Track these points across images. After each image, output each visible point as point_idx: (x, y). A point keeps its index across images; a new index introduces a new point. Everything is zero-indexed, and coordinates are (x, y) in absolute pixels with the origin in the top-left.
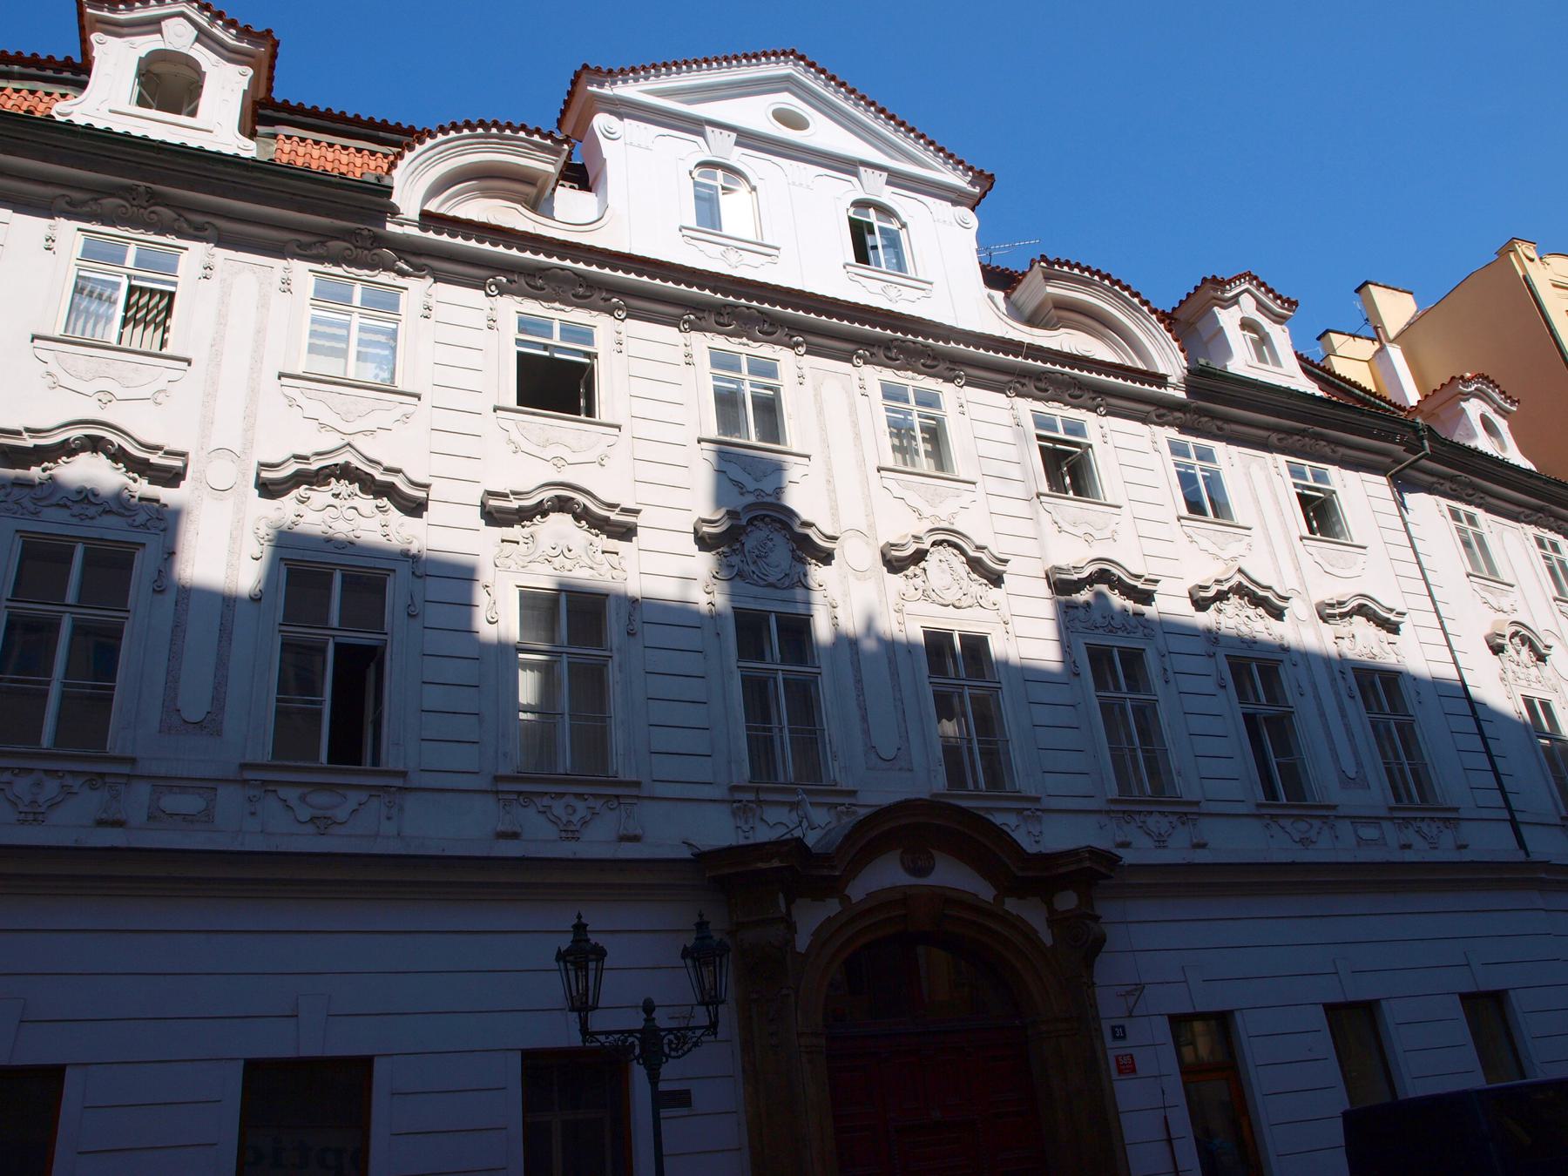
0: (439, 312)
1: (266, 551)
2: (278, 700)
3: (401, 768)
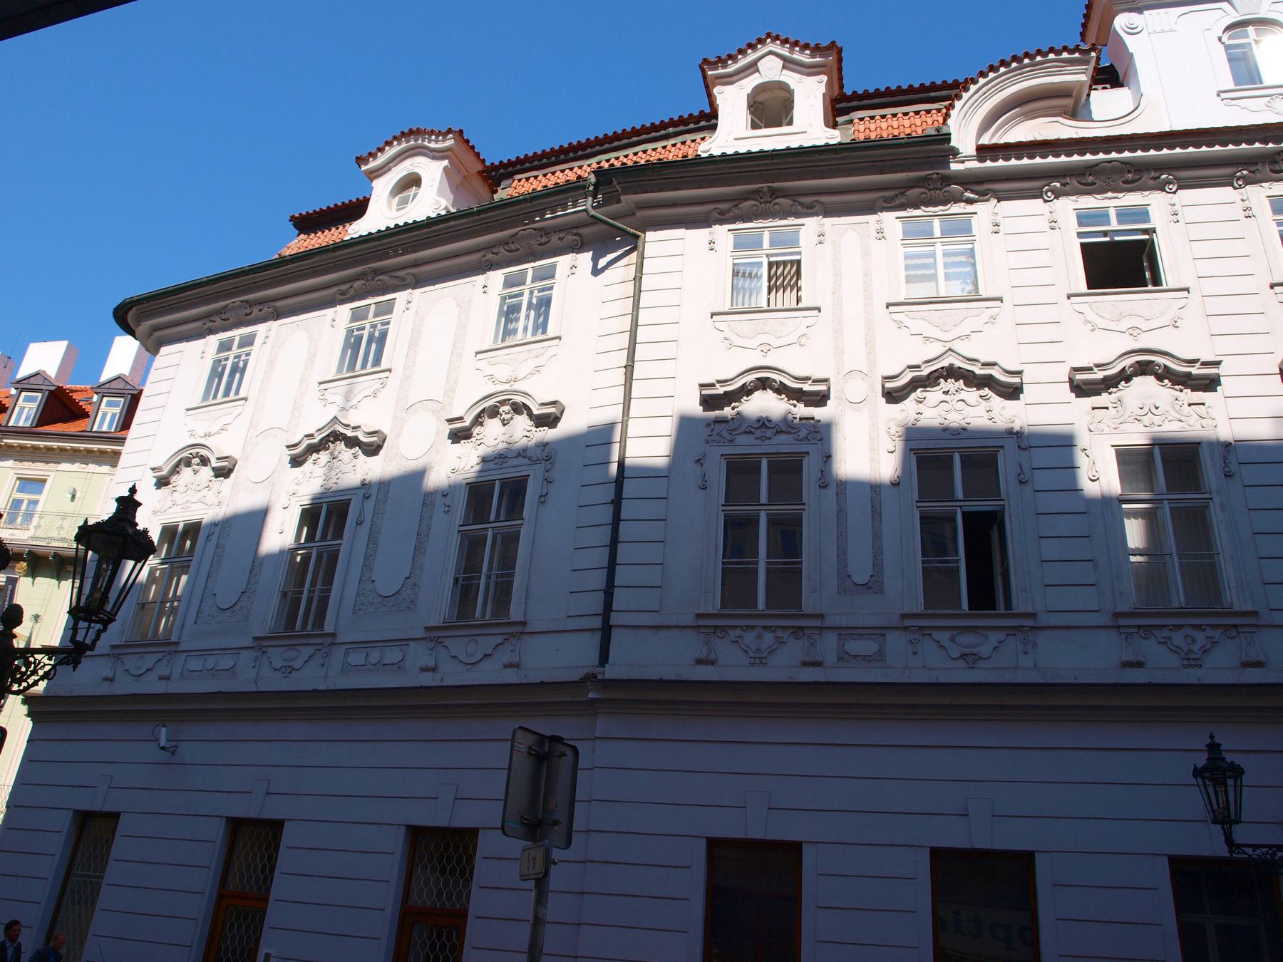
0: (1006, 226)
1: (899, 445)
2: (923, 562)
3: (1030, 610)
